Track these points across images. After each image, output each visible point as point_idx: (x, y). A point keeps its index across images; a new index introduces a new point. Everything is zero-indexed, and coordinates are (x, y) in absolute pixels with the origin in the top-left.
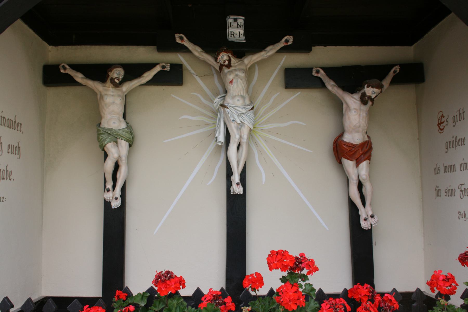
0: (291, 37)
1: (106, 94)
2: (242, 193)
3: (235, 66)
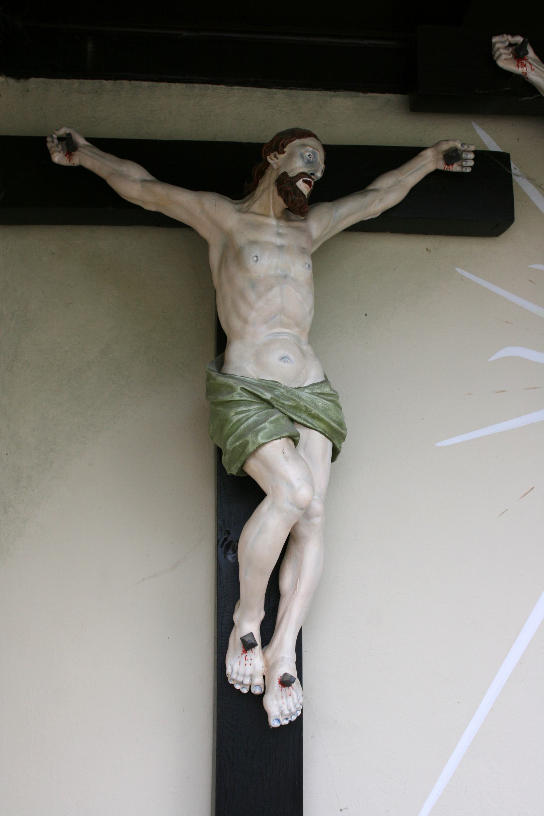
1: (254, 243)
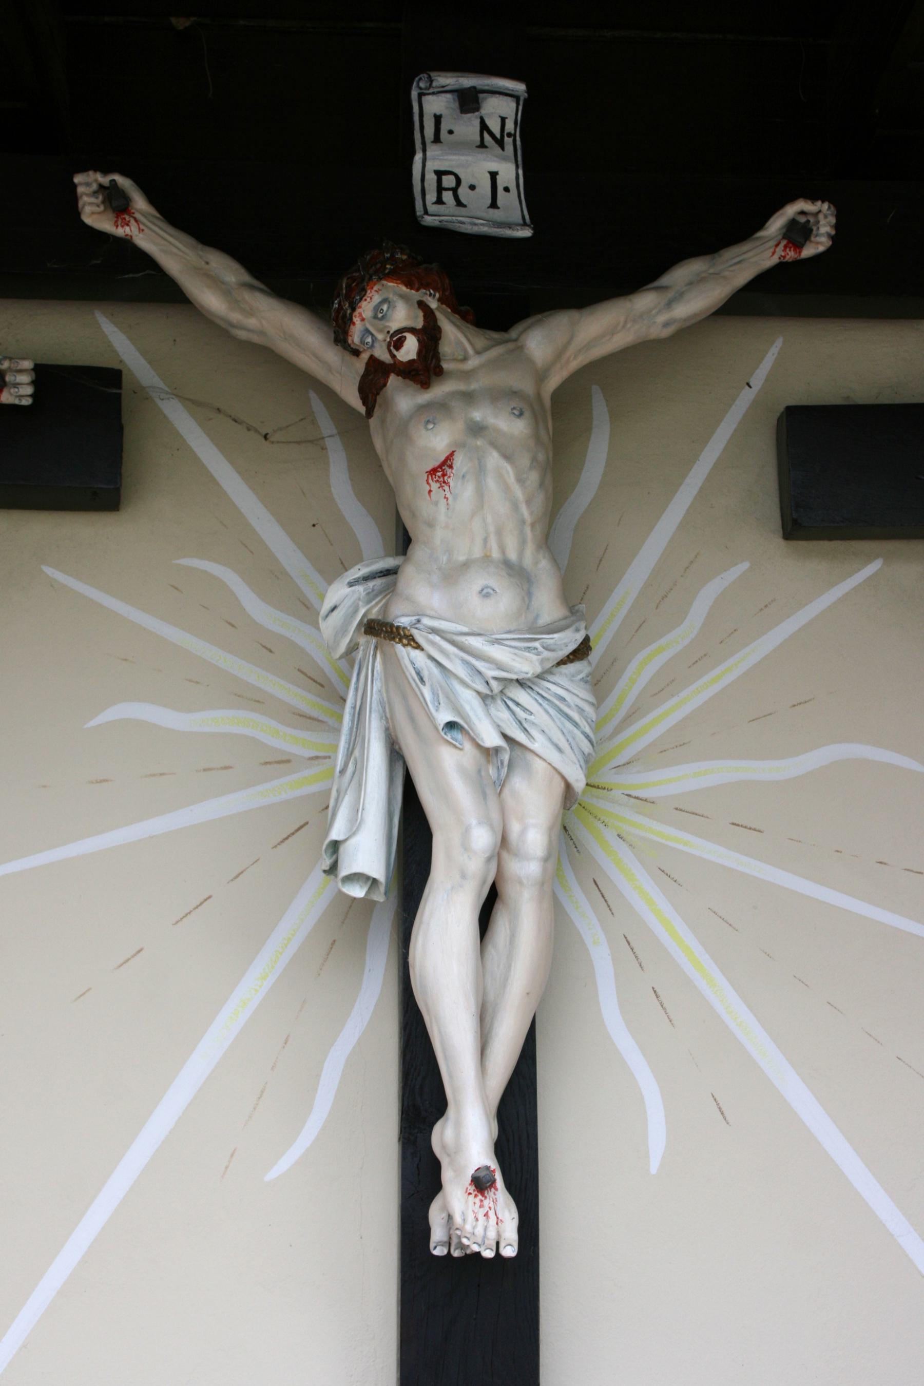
0: (826, 206)
2: (509, 1251)
3: (467, 375)
